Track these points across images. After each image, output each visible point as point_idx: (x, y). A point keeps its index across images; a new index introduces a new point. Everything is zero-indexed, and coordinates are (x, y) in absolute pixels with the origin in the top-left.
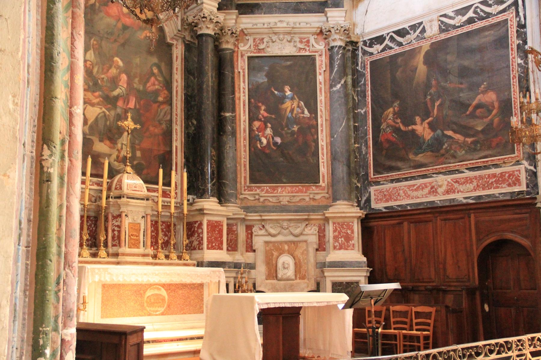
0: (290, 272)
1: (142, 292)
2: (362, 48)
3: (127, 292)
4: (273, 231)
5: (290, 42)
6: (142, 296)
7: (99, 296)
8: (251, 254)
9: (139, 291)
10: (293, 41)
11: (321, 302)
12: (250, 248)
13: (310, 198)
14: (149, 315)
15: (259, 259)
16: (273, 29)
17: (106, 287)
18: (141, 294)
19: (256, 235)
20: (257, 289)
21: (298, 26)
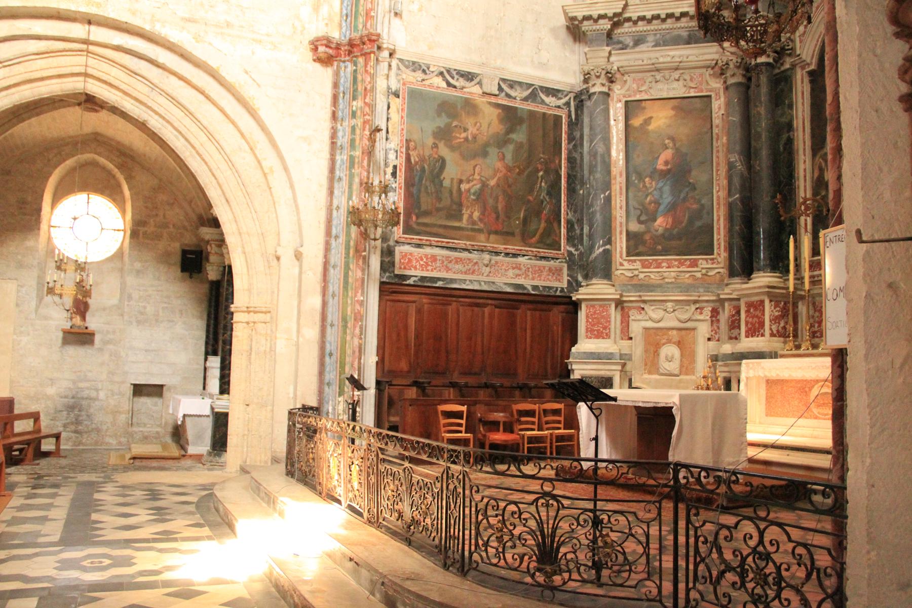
0: (674, 367)
1: (807, 389)
2: (570, 98)
3: (790, 389)
4: (654, 315)
5: (678, 80)
6: (807, 394)
7: (763, 392)
8: (627, 343)
9: (803, 389)
10: (681, 78)
11: (648, 402)
13: (702, 275)
14: (816, 418)
15: (637, 349)
16: (656, 65)
17: (771, 383)
18: (806, 392)
19: (633, 320)
20: (633, 386)
21: (685, 59)
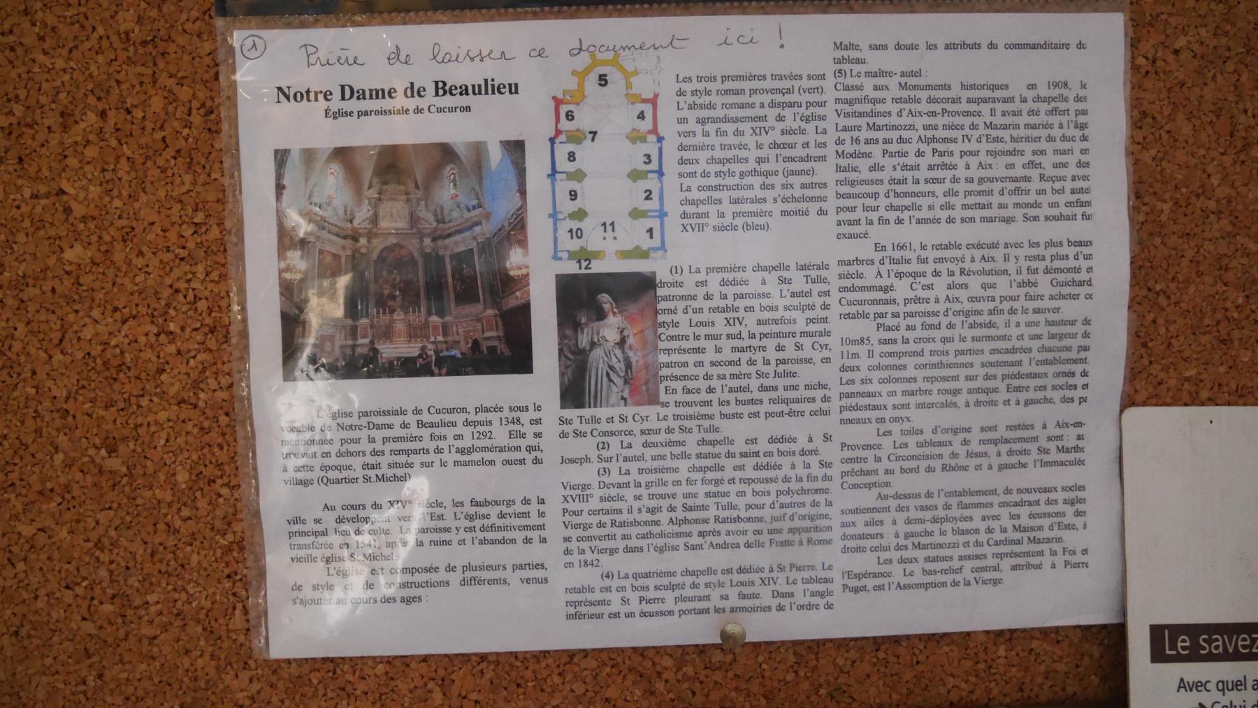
0: (329, 349)
12: (458, 334)
